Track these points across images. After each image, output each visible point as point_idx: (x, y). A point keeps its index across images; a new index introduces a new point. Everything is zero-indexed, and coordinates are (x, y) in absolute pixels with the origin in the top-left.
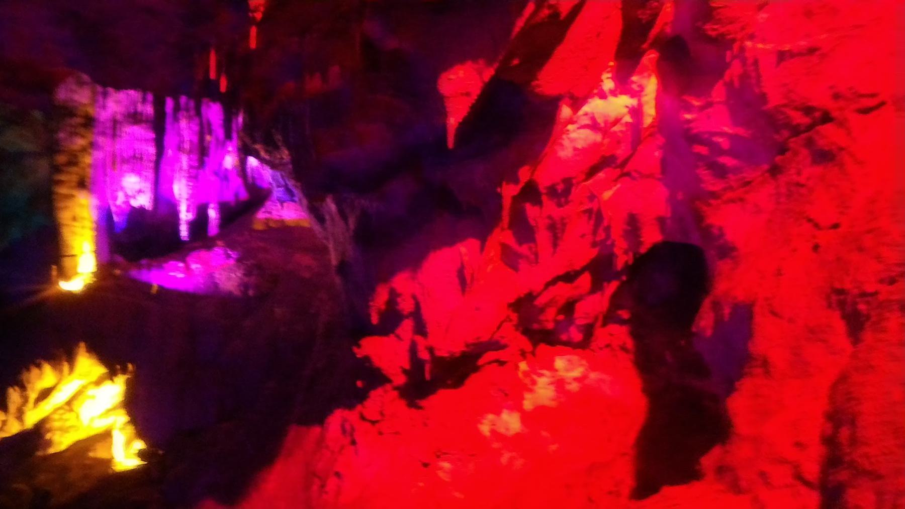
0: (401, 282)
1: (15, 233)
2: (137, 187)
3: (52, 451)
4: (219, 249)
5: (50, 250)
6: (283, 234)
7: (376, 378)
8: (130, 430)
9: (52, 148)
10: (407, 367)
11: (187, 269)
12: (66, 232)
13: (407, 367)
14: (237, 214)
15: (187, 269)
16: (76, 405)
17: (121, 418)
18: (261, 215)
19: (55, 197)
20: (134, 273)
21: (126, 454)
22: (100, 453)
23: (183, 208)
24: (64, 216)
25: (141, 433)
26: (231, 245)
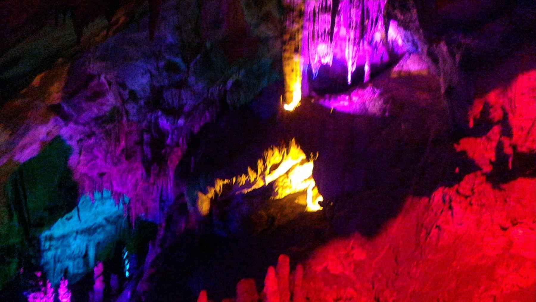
0: (492, 97)
1: (264, 83)
2: (325, 52)
3: (278, 197)
4: (369, 89)
5: (280, 88)
6: (409, 79)
7: (469, 166)
8: (316, 190)
9: (283, 31)
10: (493, 159)
11: (350, 99)
12: (288, 79)
13: (493, 159)
14: (380, 71)
15: (350, 99)
16: (290, 174)
17: (313, 183)
18: (396, 69)
19: (283, 59)
20: (321, 101)
21: (313, 203)
22: (300, 201)
23: (350, 64)
24: (287, 69)
25: (321, 192)
26: (376, 86)
